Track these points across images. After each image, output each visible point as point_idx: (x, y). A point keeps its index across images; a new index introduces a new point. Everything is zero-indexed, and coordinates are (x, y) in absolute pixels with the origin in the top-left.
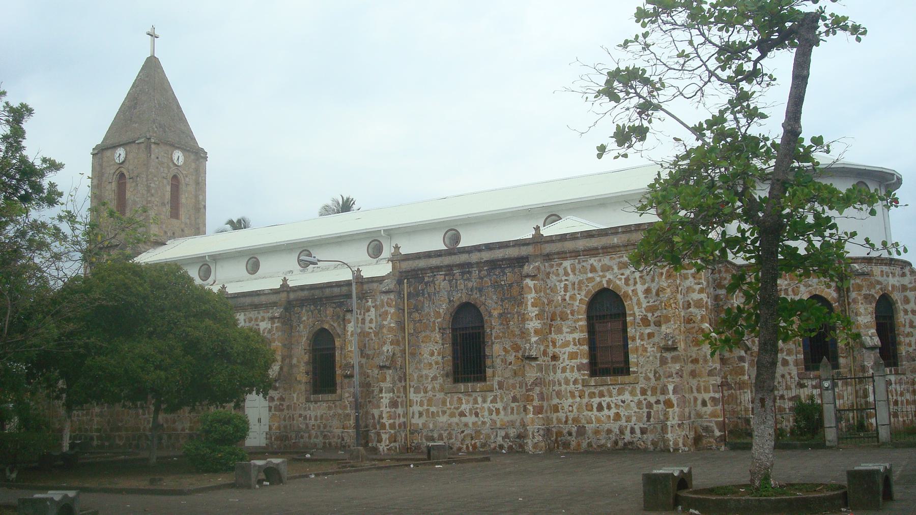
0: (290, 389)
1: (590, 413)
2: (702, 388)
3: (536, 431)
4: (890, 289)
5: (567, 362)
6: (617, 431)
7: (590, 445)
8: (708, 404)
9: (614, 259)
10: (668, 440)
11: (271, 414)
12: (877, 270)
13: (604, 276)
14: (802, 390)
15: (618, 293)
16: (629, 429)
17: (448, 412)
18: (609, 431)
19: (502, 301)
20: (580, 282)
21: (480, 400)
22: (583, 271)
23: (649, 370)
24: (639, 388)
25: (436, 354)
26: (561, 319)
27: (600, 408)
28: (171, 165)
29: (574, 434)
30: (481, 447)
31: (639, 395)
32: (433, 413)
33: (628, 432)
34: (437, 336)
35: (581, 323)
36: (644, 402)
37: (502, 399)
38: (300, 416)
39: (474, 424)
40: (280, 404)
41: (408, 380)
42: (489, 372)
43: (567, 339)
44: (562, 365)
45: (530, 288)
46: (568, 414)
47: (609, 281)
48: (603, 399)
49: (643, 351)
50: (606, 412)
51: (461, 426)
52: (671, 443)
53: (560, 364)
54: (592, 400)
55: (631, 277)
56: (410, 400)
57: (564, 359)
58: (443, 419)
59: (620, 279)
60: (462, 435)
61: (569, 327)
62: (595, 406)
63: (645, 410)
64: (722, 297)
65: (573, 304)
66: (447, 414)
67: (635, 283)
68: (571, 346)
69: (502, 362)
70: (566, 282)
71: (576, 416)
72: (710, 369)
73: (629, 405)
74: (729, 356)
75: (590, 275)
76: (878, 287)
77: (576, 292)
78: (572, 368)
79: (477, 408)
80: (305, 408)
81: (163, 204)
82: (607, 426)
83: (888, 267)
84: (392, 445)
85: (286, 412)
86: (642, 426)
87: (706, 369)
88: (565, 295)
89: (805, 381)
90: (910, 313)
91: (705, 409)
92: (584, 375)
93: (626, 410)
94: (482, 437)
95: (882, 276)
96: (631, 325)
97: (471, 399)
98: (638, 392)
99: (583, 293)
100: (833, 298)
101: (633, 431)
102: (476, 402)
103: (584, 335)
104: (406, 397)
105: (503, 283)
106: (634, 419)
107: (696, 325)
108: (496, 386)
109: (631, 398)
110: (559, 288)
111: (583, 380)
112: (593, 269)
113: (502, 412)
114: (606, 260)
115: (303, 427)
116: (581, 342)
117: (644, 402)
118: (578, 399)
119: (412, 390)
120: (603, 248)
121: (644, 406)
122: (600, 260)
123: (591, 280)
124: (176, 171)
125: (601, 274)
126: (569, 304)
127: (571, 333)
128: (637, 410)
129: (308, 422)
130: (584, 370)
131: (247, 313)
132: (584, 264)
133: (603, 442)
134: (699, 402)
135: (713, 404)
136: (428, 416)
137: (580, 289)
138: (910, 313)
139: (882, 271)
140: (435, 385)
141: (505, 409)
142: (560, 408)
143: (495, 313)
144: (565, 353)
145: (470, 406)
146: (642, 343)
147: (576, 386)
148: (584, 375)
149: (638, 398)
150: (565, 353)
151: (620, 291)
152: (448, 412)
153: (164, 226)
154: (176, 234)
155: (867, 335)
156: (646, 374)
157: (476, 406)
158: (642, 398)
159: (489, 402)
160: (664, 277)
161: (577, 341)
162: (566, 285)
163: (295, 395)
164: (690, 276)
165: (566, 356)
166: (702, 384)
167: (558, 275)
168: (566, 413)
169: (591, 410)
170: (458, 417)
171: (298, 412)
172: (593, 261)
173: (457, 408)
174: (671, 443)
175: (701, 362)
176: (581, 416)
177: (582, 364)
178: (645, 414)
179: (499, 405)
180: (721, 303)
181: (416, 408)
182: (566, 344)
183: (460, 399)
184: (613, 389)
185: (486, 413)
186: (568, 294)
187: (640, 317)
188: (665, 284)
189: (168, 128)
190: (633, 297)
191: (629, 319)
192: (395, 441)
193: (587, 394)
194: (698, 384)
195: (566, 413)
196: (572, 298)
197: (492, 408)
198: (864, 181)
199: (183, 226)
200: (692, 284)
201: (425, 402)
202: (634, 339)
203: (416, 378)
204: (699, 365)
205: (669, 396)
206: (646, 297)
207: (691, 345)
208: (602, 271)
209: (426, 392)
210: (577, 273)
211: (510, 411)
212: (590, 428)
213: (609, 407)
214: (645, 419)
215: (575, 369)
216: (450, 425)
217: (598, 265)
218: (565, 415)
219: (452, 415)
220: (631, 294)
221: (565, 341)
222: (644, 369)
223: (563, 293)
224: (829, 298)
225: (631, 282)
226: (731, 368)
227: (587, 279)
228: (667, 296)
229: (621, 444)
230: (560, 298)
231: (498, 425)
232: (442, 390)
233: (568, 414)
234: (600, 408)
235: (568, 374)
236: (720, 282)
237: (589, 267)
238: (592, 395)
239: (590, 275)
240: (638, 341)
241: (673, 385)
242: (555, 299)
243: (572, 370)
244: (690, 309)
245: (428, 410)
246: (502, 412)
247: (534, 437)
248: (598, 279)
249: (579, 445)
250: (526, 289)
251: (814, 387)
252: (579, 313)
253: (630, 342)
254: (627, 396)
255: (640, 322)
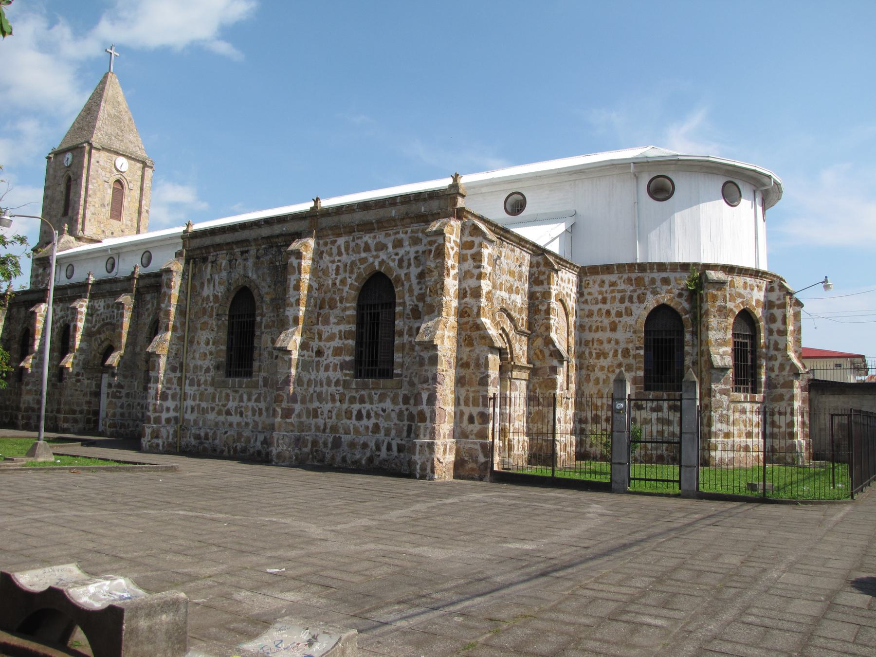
0: (132, 376)
1: (348, 422)
2: (471, 399)
3: (281, 437)
4: (754, 303)
5: (331, 359)
6: (372, 445)
7: (344, 459)
8: (476, 421)
9: (390, 235)
10: (415, 463)
11: (109, 400)
12: (739, 281)
13: (377, 257)
14: (638, 413)
15: (389, 277)
16: (385, 444)
17: (216, 409)
18: (365, 446)
19: (275, 284)
20: (353, 263)
21: (245, 397)
22: (357, 250)
23: (414, 374)
24: (402, 395)
25: (211, 343)
26: (330, 307)
27: (359, 416)
28: (114, 170)
29: (330, 445)
30: (241, 452)
31: (401, 403)
32: (203, 408)
33: (384, 448)
34: (213, 322)
35: (348, 313)
36: (406, 413)
37: (265, 397)
38: (139, 404)
39: (239, 424)
40: (117, 391)
41: (184, 371)
42: (256, 364)
43: (333, 331)
44: (325, 362)
45: (294, 267)
46: (327, 420)
47: (382, 262)
48: (363, 405)
49: (410, 349)
50: (365, 421)
51: (227, 425)
52: (418, 467)
53: (324, 361)
54: (352, 406)
55: (405, 258)
56: (185, 393)
57: (328, 355)
58: (211, 416)
59: (394, 260)
60: (226, 436)
61: (336, 317)
62: (355, 413)
63: (406, 422)
64: (538, 295)
65: (342, 290)
66: (215, 411)
67: (409, 265)
68: (337, 340)
69: (269, 355)
70: (339, 264)
71: (334, 424)
72: (482, 376)
73: (389, 415)
74: (540, 366)
75: (363, 255)
76: (739, 300)
77: (347, 275)
78: (335, 365)
79: (242, 407)
80: (143, 397)
81: (103, 205)
82: (362, 440)
83: (753, 279)
84: (153, 441)
85: (124, 400)
86: (400, 442)
87: (476, 376)
88: (336, 279)
89: (644, 403)
90: (775, 333)
91: (471, 427)
92: (346, 375)
93: (386, 421)
94: (243, 440)
95: (745, 288)
96: (400, 317)
97: (237, 396)
98: (400, 400)
99: (354, 276)
100: (684, 309)
101: (389, 448)
102: (241, 400)
103: (353, 327)
104: (181, 389)
105: (278, 264)
106: (393, 432)
107: (470, 319)
108: (261, 383)
109: (392, 407)
110: (330, 270)
111: (344, 381)
112: (367, 249)
113: (264, 413)
114: (381, 237)
115: (140, 415)
116: (346, 335)
117: (406, 413)
118: (338, 404)
119: (187, 382)
120: (379, 222)
121: (406, 417)
122: (375, 237)
123: (363, 260)
124: (119, 176)
125: (374, 253)
126: (339, 289)
127: (338, 324)
128: (398, 422)
129: (144, 411)
130: (346, 370)
131: (106, 300)
132: (359, 242)
133: (358, 457)
134: (466, 417)
135: (480, 421)
136: (199, 412)
137: (351, 272)
138: (775, 333)
139: (745, 283)
140: (208, 378)
141: (267, 409)
142: (319, 412)
143: (267, 299)
144: (329, 348)
145: (236, 404)
146: (410, 339)
147: (338, 388)
148: (346, 375)
149: (399, 407)
150: (329, 348)
151: (392, 275)
152: (216, 409)
153: (102, 226)
154: (115, 234)
155: (718, 354)
156: (411, 377)
157: (241, 404)
158: (404, 407)
159: (253, 401)
160: (432, 256)
161: (343, 334)
162: (338, 267)
163: (136, 384)
164: (469, 257)
165: (330, 352)
166: (471, 395)
167: (331, 255)
168: (325, 419)
169: (350, 418)
170: (224, 415)
171: (138, 401)
172: (367, 238)
173: (224, 406)
174: (418, 467)
175: (472, 367)
176: (339, 424)
177: (345, 361)
178: (405, 428)
179: (262, 405)
180: (537, 302)
181: (189, 403)
182: (331, 338)
183: (228, 395)
184: (375, 394)
185: (250, 413)
186: (339, 277)
187: (411, 307)
188: (433, 265)
189: (115, 137)
190: (405, 283)
191: (398, 309)
192: (157, 437)
193: (347, 398)
194: (467, 395)
195: (325, 419)
196: (343, 282)
197: (255, 407)
198: (736, 182)
199: (123, 227)
200: (472, 267)
201: (198, 396)
202: (401, 334)
203: (191, 369)
204: (470, 371)
205: (422, 407)
206: (419, 283)
207: (463, 344)
208: (376, 250)
209: (199, 385)
210: (351, 253)
211: (271, 412)
212: (345, 438)
213: (369, 416)
214: (405, 434)
215: (338, 367)
216: (217, 424)
217: (372, 243)
218: (324, 422)
219: (219, 413)
220: (403, 279)
221: (332, 333)
222: (410, 371)
223: (334, 276)
224: (679, 309)
225: (405, 264)
226: (541, 380)
227: (360, 260)
228: (433, 279)
229: (376, 462)
230: (330, 282)
231: (260, 428)
232: (213, 384)
233: (327, 420)
234: (359, 416)
235: (331, 373)
236: (538, 277)
237: (363, 245)
238: (352, 400)
239: (363, 255)
240: (406, 337)
241: (427, 394)
242: (326, 283)
243: (335, 370)
244: (466, 299)
245: (199, 405)
246: (264, 413)
247: (278, 446)
248: (371, 260)
249: (333, 458)
250: (290, 269)
251: (653, 410)
252: (347, 300)
253: (396, 338)
254: (388, 404)
255: (410, 313)
